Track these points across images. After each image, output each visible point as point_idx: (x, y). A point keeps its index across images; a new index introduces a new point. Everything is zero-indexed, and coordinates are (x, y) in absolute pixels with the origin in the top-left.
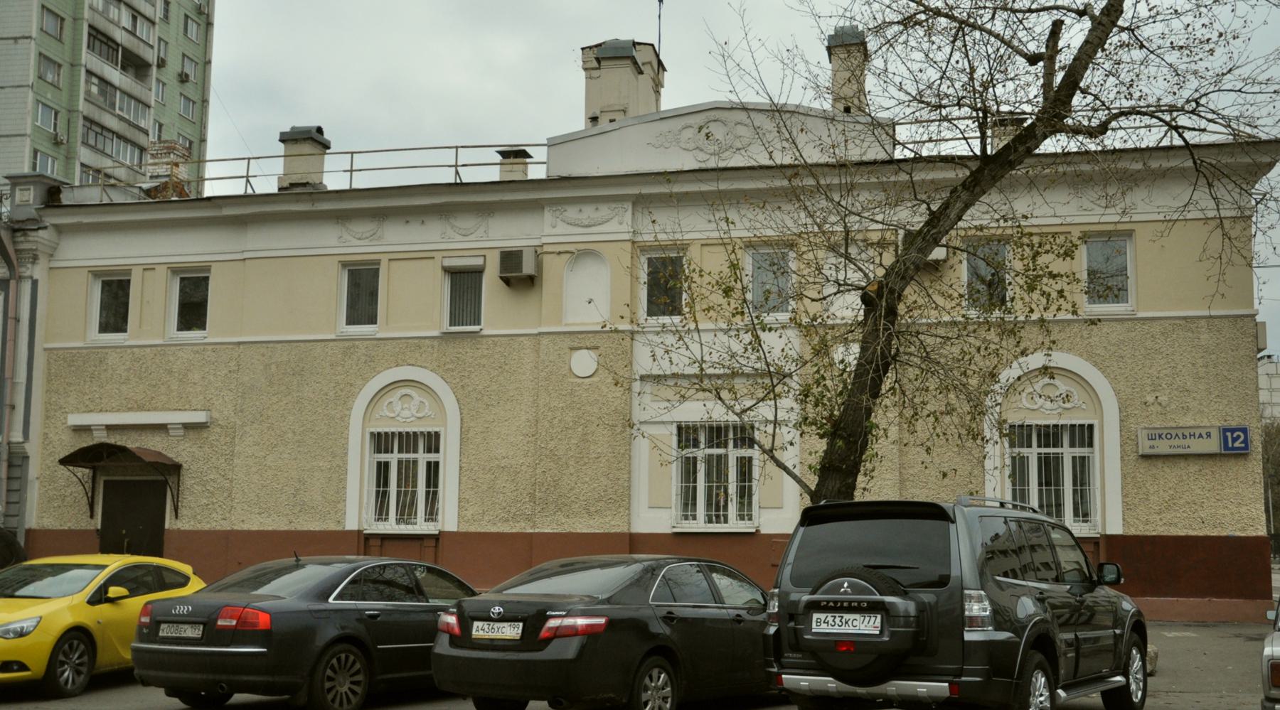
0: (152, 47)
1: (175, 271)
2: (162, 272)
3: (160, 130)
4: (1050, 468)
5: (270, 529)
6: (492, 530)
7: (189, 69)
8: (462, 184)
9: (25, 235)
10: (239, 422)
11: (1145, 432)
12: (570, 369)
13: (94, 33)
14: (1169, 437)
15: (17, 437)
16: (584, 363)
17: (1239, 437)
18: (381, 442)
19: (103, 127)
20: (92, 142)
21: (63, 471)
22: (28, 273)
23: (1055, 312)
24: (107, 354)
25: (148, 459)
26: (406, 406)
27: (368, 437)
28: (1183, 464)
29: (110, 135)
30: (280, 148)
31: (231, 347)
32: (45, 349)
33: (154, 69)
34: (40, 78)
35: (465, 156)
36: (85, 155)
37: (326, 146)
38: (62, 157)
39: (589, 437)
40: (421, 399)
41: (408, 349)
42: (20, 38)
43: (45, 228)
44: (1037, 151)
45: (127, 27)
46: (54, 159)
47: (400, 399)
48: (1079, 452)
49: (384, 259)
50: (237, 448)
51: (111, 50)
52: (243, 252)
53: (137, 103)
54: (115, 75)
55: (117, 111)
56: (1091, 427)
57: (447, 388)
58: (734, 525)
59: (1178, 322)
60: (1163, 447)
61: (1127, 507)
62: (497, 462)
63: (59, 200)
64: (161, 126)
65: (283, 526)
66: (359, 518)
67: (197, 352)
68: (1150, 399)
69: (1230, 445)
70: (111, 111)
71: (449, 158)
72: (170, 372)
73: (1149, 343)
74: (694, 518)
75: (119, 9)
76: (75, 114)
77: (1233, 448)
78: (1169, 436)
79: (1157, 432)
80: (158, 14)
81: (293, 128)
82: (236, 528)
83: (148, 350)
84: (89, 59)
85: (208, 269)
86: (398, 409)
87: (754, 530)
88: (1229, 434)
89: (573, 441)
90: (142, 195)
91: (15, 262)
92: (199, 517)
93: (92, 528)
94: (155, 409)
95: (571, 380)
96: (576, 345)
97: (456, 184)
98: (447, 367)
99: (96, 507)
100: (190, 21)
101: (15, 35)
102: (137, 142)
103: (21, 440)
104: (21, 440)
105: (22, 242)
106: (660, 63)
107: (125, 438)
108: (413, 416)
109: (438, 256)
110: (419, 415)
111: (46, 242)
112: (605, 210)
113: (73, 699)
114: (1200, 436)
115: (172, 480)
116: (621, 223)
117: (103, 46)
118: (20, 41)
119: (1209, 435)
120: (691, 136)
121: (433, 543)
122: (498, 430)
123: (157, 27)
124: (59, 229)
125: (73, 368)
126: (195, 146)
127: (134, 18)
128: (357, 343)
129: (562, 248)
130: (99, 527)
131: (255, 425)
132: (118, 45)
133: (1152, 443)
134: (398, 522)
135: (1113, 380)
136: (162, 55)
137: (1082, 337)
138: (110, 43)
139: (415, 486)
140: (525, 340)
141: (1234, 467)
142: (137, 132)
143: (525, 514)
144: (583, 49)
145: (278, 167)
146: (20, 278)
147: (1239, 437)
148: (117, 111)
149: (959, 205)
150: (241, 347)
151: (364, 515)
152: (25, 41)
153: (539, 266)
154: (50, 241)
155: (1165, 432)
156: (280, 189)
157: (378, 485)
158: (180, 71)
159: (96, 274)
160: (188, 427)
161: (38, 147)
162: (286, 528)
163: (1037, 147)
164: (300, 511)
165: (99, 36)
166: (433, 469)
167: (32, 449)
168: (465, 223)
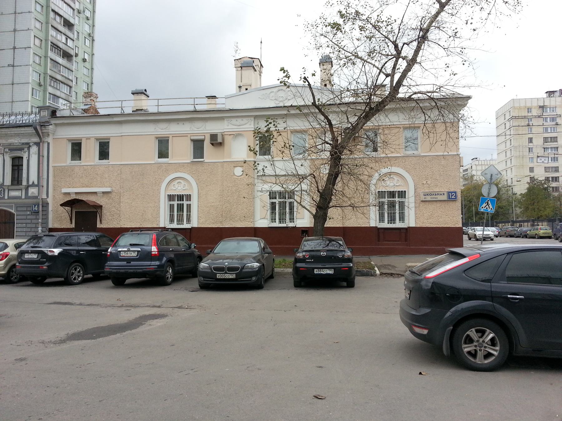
1: (97, 139)
2: (93, 140)
3: (77, 80)
4: (180, 208)
5: (134, 227)
7: (86, 57)
9: (45, 127)
13: (52, 45)
14: (431, 195)
15: (44, 196)
16: (238, 171)
17: (453, 195)
18: (171, 198)
19: (56, 79)
20: (52, 85)
21: (62, 208)
22: (46, 140)
23: (476, 2)
24: (74, 168)
25: (91, 204)
26: (179, 186)
27: (167, 196)
28: (435, 203)
29: (59, 82)
31: (118, 166)
32: (53, 166)
33: (74, 57)
36: (50, 90)
38: (42, 91)
39: (240, 196)
40: (398, 179)
41: (180, 166)
42: (27, 48)
43: (52, 124)
45: (64, 42)
46: (39, 91)
47: (177, 183)
48: (401, 200)
49: (171, 136)
50: (122, 200)
51: (58, 51)
52: (121, 133)
53: (68, 70)
54: (60, 60)
55: (61, 73)
56: (405, 191)
59: (434, 157)
60: (429, 198)
61: (416, 218)
62: (210, 204)
64: (77, 78)
66: (165, 223)
67: (106, 167)
68: (425, 182)
70: (59, 73)
71: (119, 104)
72: (97, 174)
73: (425, 164)
74: (275, 222)
75: (61, 36)
76: (46, 75)
77: (452, 198)
78: (431, 195)
79: (427, 193)
82: (122, 227)
83: (89, 167)
84: (51, 54)
85: (109, 139)
86: (177, 187)
87: (295, 226)
88: (450, 194)
90: (83, 112)
91: (42, 137)
92: (109, 223)
94: (92, 187)
95: (234, 177)
98: (193, 172)
100: (86, 39)
101: (25, 47)
102: (68, 84)
103: (46, 198)
104: (46, 198)
106: (261, 65)
107: (82, 197)
108: (182, 189)
109: (189, 135)
110: (184, 189)
112: (245, 120)
113: (70, 286)
114: (441, 194)
115: (99, 210)
116: (250, 125)
117: (56, 49)
118: (27, 49)
119: (444, 194)
120: (273, 95)
121: (405, 231)
122: (210, 193)
125: (63, 173)
126: (90, 85)
127: (67, 39)
128: (162, 165)
129: (229, 133)
130: (74, 227)
131: (128, 192)
132: (61, 49)
133: (425, 197)
135: (413, 177)
137: (402, 162)
138: (58, 48)
140: (219, 164)
141: (452, 204)
142: (68, 80)
143: (220, 221)
146: (43, 142)
147: (453, 195)
148: (61, 73)
149: (361, 124)
150: (122, 166)
151: (166, 222)
152: (29, 49)
153: (223, 140)
154: (53, 129)
155: (429, 193)
158: (83, 58)
159: (69, 140)
160: (104, 193)
161: (34, 87)
164: (144, 221)
165: (54, 46)
166: (189, 206)
167: (50, 200)
168: (198, 124)
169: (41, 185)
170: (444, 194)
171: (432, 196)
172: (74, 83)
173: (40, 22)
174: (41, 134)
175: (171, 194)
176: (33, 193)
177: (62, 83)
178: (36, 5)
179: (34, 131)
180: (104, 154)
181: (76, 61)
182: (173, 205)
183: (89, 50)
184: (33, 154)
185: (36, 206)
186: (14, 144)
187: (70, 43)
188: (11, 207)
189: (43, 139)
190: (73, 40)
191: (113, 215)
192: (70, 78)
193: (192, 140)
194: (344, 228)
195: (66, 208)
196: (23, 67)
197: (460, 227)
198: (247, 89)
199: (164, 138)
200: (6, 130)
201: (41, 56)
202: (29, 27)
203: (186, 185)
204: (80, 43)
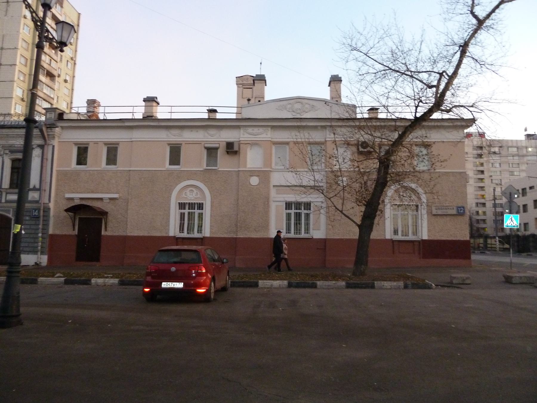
0: (56, 70)
4: (298, 216)
6: (222, 236)
7: (68, 78)
8: (210, 119)
9: (51, 129)
10: (130, 198)
11: (434, 207)
12: (250, 183)
14: (441, 209)
15: (46, 201)
18: (182, 206)
22: (51, 143)
26: (191, 194)
27: (178, 205)
30: (143, 104)
33: (57, 78)
34: (19, 78)
35: (174, 109)
37: (158, 104)
41: (191, 175)
44: (431, 118)
48: (306, 211)
49: (183, 143)
57: (206, 188)
58: (303, 235)
60: (440, 212)
61: (429, 231)
63: (63, 117)
65: (146, 234)
69: (459, 212)
77: (460, 213)
80: (59, 60)
81: (147, 97)
85: (181, 144)
88: (459, 209)
89: (250, 207)
90: (88, 117)
93: (74, 234)
96: (251, 175)
97: (132, 119)
99: (75, 226)
104: (48, 202)
105: (49, 132)
110: (196, 197)
111: (58, 132)
112: (261, 130)
119: (453, 209)
121: (417, 243)
123: (58, 63)
124: (62, 128)
130: (77, 234)
132: (45, 69)
134: (188, 233)
136: (59, 73)
139: (194, 221)
141: (460, 218)
144: (236, 77)
145: (143, 110)
153: (239, 148)
155: (440, 207)
156: (143, 117)
157: (181, 220)
160: (111, 199)
162: (147, 235)
163: (431, 116)
166: (201, 216)
167: (51, 205)
168: (212, 132)
169: (44, 189)
170: (453, 209)
171: (443, 211)
172: (55, 101)
173: (27, 42)
174: (46, 136)
175: (183, 202)
176: (33, 197)
177: (44, 100)
178: (24, 26)
179: (39, 133)
180: (112, 159)
181: (59, 81)
182: (184, 213)
183: (70, 73)
184: (36, 156)
185: (37, 211)
186: (16, 146)
187: (53, 64)
188: (8, 211)
189: (48, 142)
190: (57, 62)
191: (120, 223)
192: (52, 96)
193: (206, 148)
194: (236, 238)
195: (70, 213)
196: (7, 82)
197: (468, 240)
198: (259, 101)
199: (177, 145)
200: (7, 131)
201: (26, 74)
202: (15, 46)
203: (199, 193)
204: (63, 65)
